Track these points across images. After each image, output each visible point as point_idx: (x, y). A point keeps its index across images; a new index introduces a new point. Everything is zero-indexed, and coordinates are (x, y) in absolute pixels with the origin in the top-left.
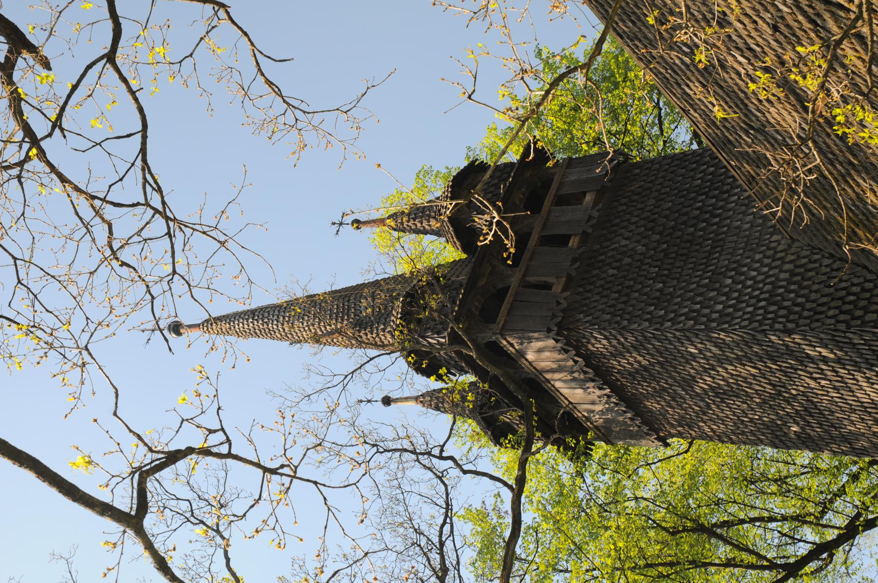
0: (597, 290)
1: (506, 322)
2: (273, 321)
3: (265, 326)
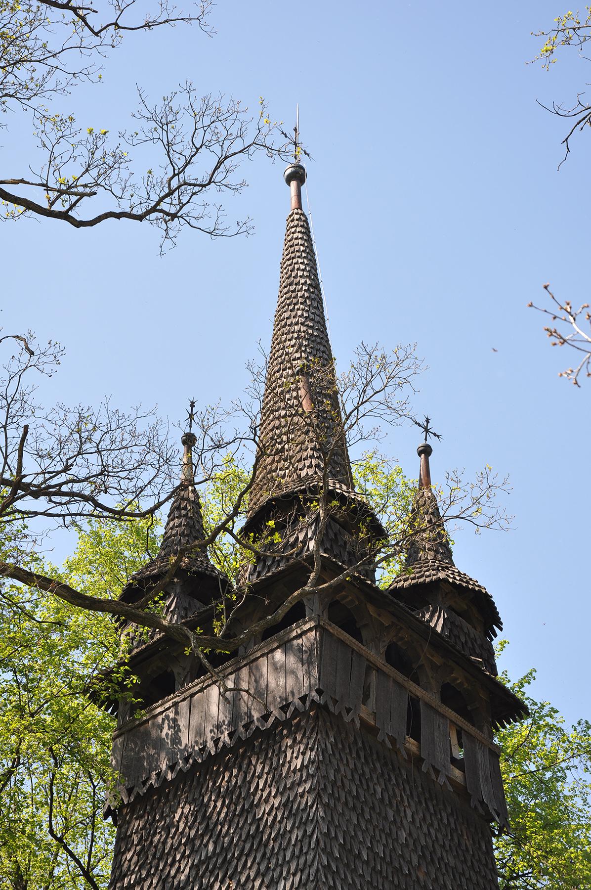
0: (359, 765)
1: (332, 635)
2: (307, 311)
3: (301, 300)
